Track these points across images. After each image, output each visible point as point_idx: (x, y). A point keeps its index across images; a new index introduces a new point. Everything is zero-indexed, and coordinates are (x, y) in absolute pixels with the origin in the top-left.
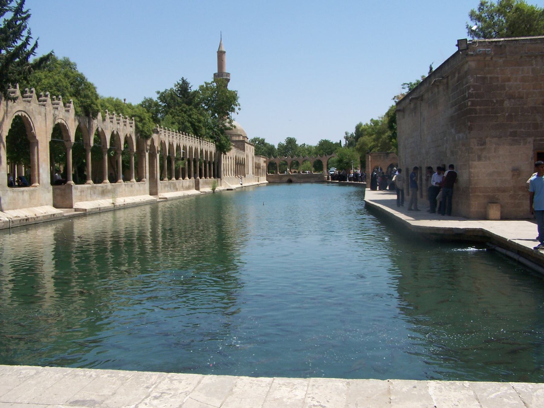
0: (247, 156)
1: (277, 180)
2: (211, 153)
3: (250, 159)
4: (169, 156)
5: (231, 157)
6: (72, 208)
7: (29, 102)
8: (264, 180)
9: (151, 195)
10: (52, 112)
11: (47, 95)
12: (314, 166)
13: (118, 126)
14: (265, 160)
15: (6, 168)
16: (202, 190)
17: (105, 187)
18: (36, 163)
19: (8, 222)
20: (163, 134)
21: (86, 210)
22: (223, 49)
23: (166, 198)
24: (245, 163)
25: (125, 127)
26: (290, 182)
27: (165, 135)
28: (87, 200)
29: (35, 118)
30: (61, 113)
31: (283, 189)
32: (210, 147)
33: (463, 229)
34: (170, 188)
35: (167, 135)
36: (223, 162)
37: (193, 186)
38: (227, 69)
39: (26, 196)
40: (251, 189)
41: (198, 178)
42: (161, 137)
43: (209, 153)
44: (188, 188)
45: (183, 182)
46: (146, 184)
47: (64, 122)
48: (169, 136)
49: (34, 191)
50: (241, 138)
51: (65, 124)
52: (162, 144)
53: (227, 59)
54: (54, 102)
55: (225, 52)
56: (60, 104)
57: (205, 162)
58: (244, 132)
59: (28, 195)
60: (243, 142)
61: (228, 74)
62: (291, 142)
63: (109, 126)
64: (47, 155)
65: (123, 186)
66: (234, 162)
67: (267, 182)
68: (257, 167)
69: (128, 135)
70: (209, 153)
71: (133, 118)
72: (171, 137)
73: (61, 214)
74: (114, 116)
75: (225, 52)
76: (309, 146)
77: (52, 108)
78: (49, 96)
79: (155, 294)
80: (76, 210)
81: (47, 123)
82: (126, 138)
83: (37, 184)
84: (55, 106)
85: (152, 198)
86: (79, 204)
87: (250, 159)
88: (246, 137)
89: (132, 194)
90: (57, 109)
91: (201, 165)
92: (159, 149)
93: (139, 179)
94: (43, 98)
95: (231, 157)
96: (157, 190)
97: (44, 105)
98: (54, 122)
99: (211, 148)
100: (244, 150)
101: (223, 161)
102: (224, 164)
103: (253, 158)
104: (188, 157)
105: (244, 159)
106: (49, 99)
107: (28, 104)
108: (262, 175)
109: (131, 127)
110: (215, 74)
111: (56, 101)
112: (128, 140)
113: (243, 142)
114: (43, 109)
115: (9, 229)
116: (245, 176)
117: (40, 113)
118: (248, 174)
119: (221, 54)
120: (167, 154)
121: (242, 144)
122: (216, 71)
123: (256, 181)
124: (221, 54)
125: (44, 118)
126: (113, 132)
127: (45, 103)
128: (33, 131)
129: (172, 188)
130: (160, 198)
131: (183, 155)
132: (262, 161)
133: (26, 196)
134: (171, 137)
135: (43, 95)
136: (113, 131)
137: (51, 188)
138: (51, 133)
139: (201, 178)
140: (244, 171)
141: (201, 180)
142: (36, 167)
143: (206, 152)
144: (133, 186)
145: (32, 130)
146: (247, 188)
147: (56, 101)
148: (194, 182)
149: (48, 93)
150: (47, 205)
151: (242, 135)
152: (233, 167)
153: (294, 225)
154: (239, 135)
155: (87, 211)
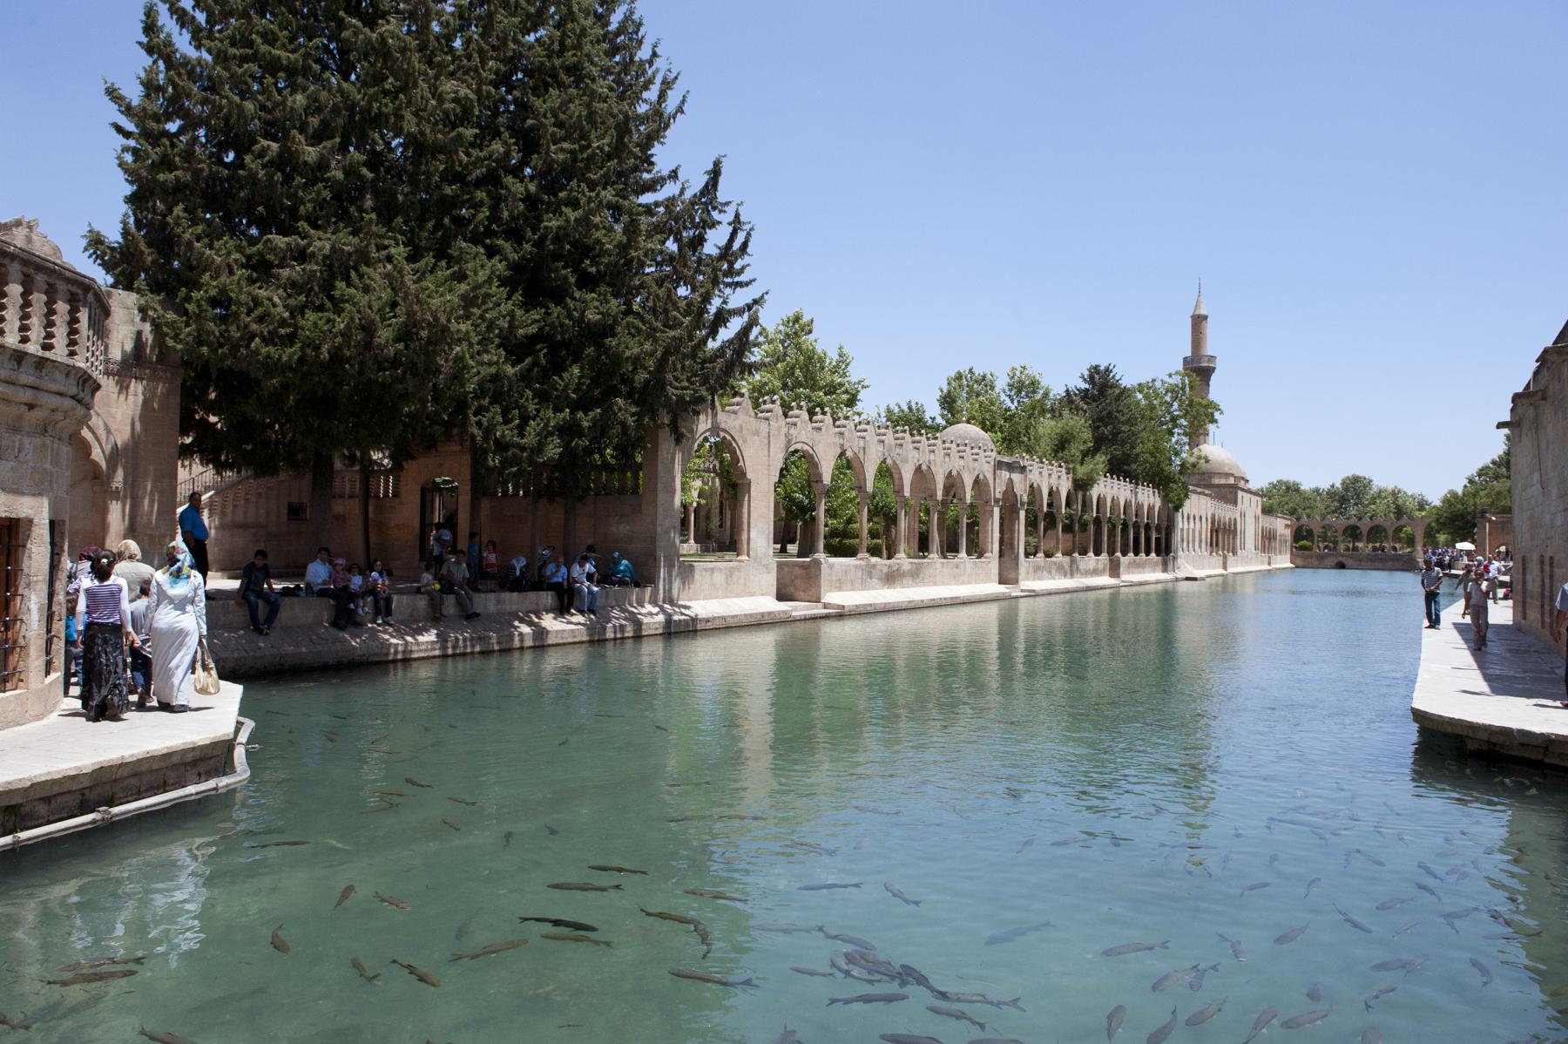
0: (1243, 515)
1: (1315, 561)
2: (1151, 508)
3: (1250, 521)
4: (1125, 520)
5: (1201, 517)
6: (818, 601)
7: (735, 413)
8: (1283, 561)
9: (1000, 583)
10: (784, 430)
12: (1356, 528)
13: (932, 457)
16: (1127, 577)
17: (895, 568)
18: (745, 521)
20: (1036, 472)
21: (843, 607)
23: (1034, 591)
24: (1235, 528)
25: (947, 459)
26: (1341, 566)
27: (1041, 473)
28: (853, 590)
29: (745, 441)
30: (803, 432)
31: (1328, 579)
32: (1148, 498)
33: (1542, 734)
34: (1050, 572)
35: (1045, 473)
36: (1180, 526)
37: (1104, 569)
40: (1249, 580)
41: (1118, 554)
42: (1030, 476)
44: (1096, 572)
46: (992, 561)
47: (809, 448)
48: (1050, 475)
49: (738, 569)
50: (1231, 481)
51: (811, 452)
52: (1034, 491)
53: (1211, 330)
54: (896, 435)
55: (1205, 318)
56: (802, 417)
57: (1148, 527)
58: (1238, 467)
59: (723, 577)
60: (1234, 489)
61: (1212, 358)
63: (910, 456)
64: (769, 506)
65: (939, 566)
66: (1209, 525)
67: (1293, 566)
71: (923, 431)
72: (1054, 476)
73: (785, 612)
75: (1205, 318)
76: (943, 408)
77: (784, 424)
78: (829, 414)
80: (826, 606)
81: (771, 450)
82: (977, 482)
83: (744, 557)
85: (1002, 589)
86: (835, 597)
87: (1250, 521)
88: (1243, 478)
89: (956, 579)
90: (795, 425)
92: (1025, 499)
94: (819, 417)
95: (1201, 517)
96: (1017, 574)
99: (1054, 481)
100: (1235, 503)
101: (1180, 523)
102: (1182, 530)
103: (1257, 518)
104: (1108, 515)
105: (1235, 520)
107: (733, 416)
108: (1280, 552)
109: (989, 463)
110: (1185, 359)
112: (1151, 508)
113: (1234, 489)
114: (763, 426)
116: (1234, 553)
119: (1198, 321)
120: (1108, 515)
121: (1231, 493)
122: (1189, 353)
123: (1262, 563)
124: (1198, 321)
125: (766, 441)
128: (741, 464)
129: (1053, 572)
130: (1022, 591)
131: (1097, 512)
133: (719, 578)
134: (1054, 476)
135: (769, 401)
136: (920, 465)
139: (1124, 554)
140: (1234, 543)
141: (1123, 559)
142: (746, 528)
144: (962, 566)
145: (738, 462)
146: (1239, 578)
148: (1107, 562)
149: (776, 397)
150: (763, 595)
151: (1233, 475)
152: (1206, 535)
154: (1227, 475)
155: (846, 609)
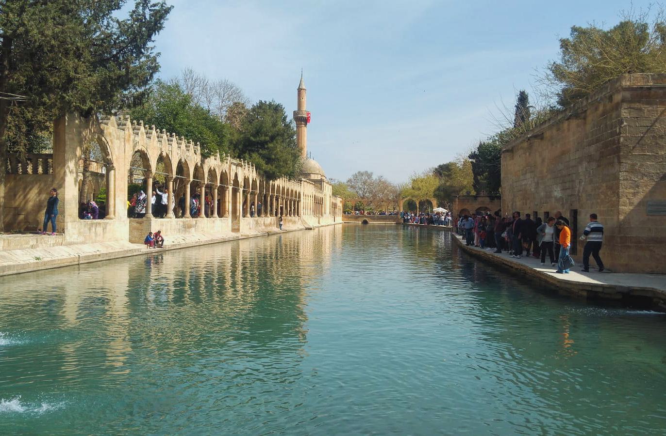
11: (127, 119)
14: (341, 200)
15: (117, 201)
19: (76, 258)
22: (304, 87)
27: (249, 170)
38: (305, 108)
39: (99, 230)
43: (294, 192)
45: (264, 219)
46: (228, 220)
62: (261, 102)
68: (334, 206)
69: (212, 169)
70: (294, 192)
74: (183, 142)
78: (142, 124)
79: (154, 381)
84: (135, 131)
87: (328, 198)
91: (290, 203)
93: (221, 214)
97: (123, 130)
98: (134, 149)
106: (129, 123)
111: (137, 127)
115: (78, 266)
117: (118, 138)
118: (325, 213)
126: (181, 160)
127: (124, 126)
130: (242, 235)
132: (339, 201)
137: (127, 220)
138: (130, 161)
143: (296, 192)
147: (123, 122)
148: (275, 219)
149: (242, 159)
153: (129, 417)
